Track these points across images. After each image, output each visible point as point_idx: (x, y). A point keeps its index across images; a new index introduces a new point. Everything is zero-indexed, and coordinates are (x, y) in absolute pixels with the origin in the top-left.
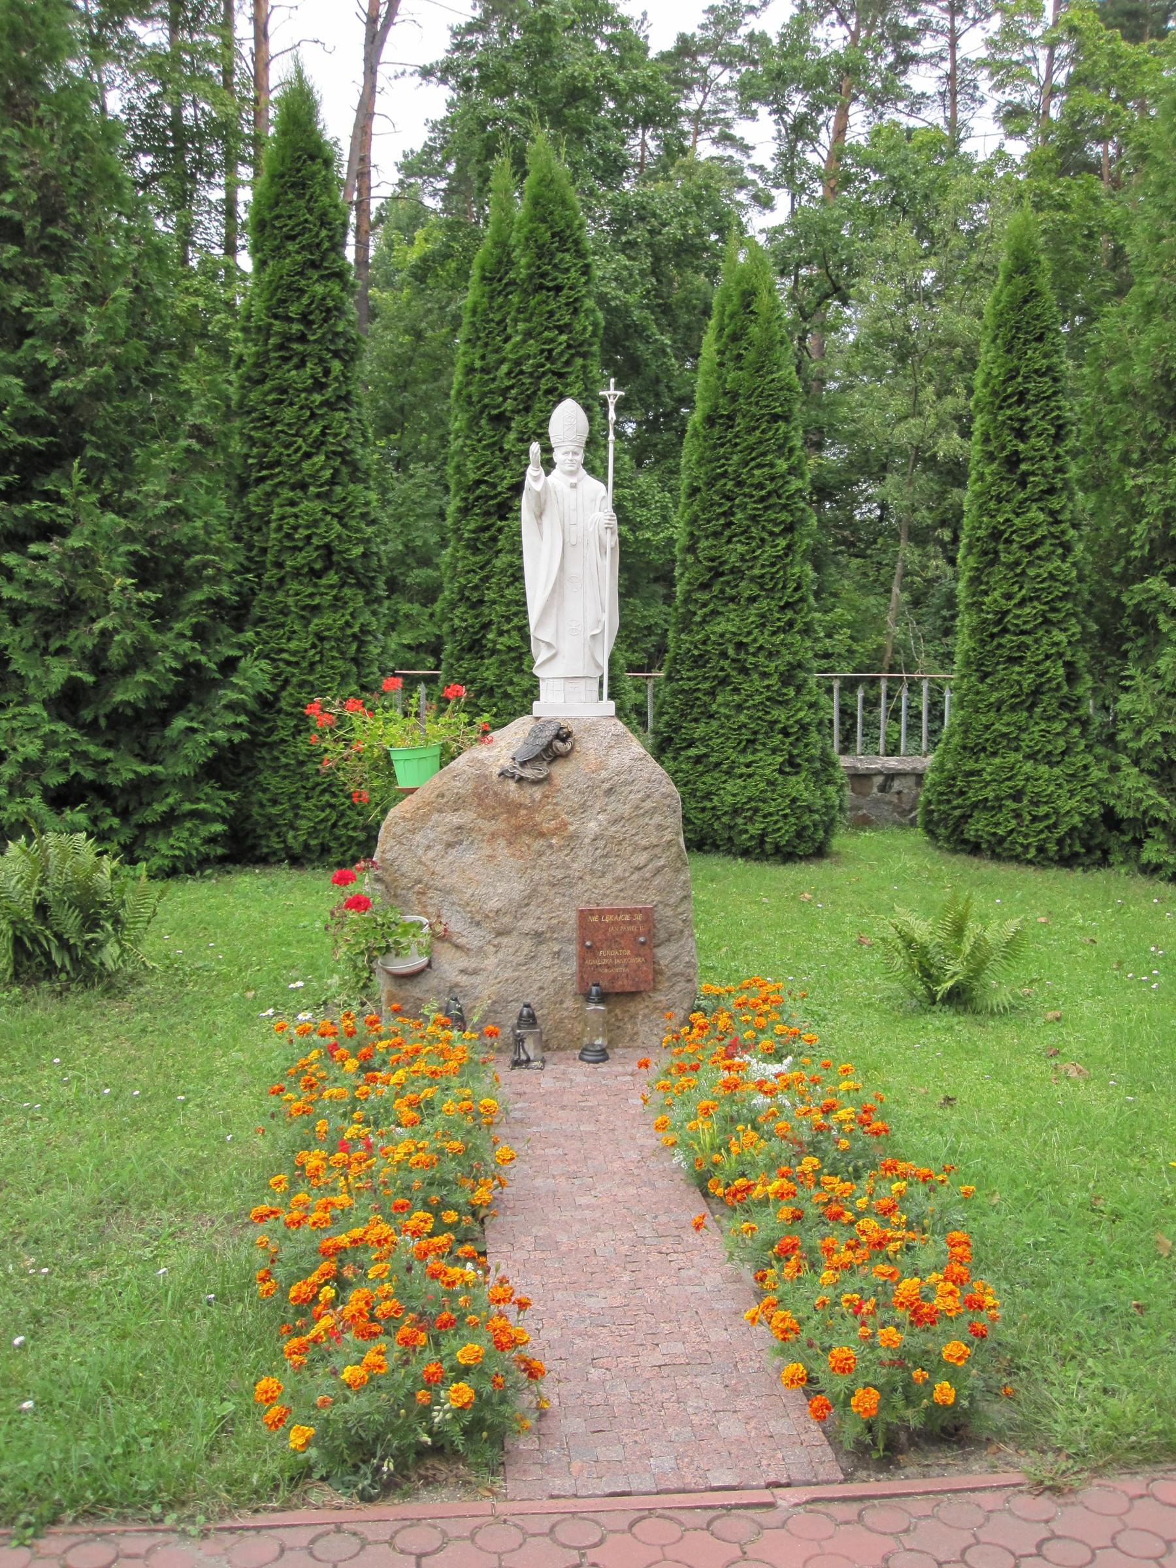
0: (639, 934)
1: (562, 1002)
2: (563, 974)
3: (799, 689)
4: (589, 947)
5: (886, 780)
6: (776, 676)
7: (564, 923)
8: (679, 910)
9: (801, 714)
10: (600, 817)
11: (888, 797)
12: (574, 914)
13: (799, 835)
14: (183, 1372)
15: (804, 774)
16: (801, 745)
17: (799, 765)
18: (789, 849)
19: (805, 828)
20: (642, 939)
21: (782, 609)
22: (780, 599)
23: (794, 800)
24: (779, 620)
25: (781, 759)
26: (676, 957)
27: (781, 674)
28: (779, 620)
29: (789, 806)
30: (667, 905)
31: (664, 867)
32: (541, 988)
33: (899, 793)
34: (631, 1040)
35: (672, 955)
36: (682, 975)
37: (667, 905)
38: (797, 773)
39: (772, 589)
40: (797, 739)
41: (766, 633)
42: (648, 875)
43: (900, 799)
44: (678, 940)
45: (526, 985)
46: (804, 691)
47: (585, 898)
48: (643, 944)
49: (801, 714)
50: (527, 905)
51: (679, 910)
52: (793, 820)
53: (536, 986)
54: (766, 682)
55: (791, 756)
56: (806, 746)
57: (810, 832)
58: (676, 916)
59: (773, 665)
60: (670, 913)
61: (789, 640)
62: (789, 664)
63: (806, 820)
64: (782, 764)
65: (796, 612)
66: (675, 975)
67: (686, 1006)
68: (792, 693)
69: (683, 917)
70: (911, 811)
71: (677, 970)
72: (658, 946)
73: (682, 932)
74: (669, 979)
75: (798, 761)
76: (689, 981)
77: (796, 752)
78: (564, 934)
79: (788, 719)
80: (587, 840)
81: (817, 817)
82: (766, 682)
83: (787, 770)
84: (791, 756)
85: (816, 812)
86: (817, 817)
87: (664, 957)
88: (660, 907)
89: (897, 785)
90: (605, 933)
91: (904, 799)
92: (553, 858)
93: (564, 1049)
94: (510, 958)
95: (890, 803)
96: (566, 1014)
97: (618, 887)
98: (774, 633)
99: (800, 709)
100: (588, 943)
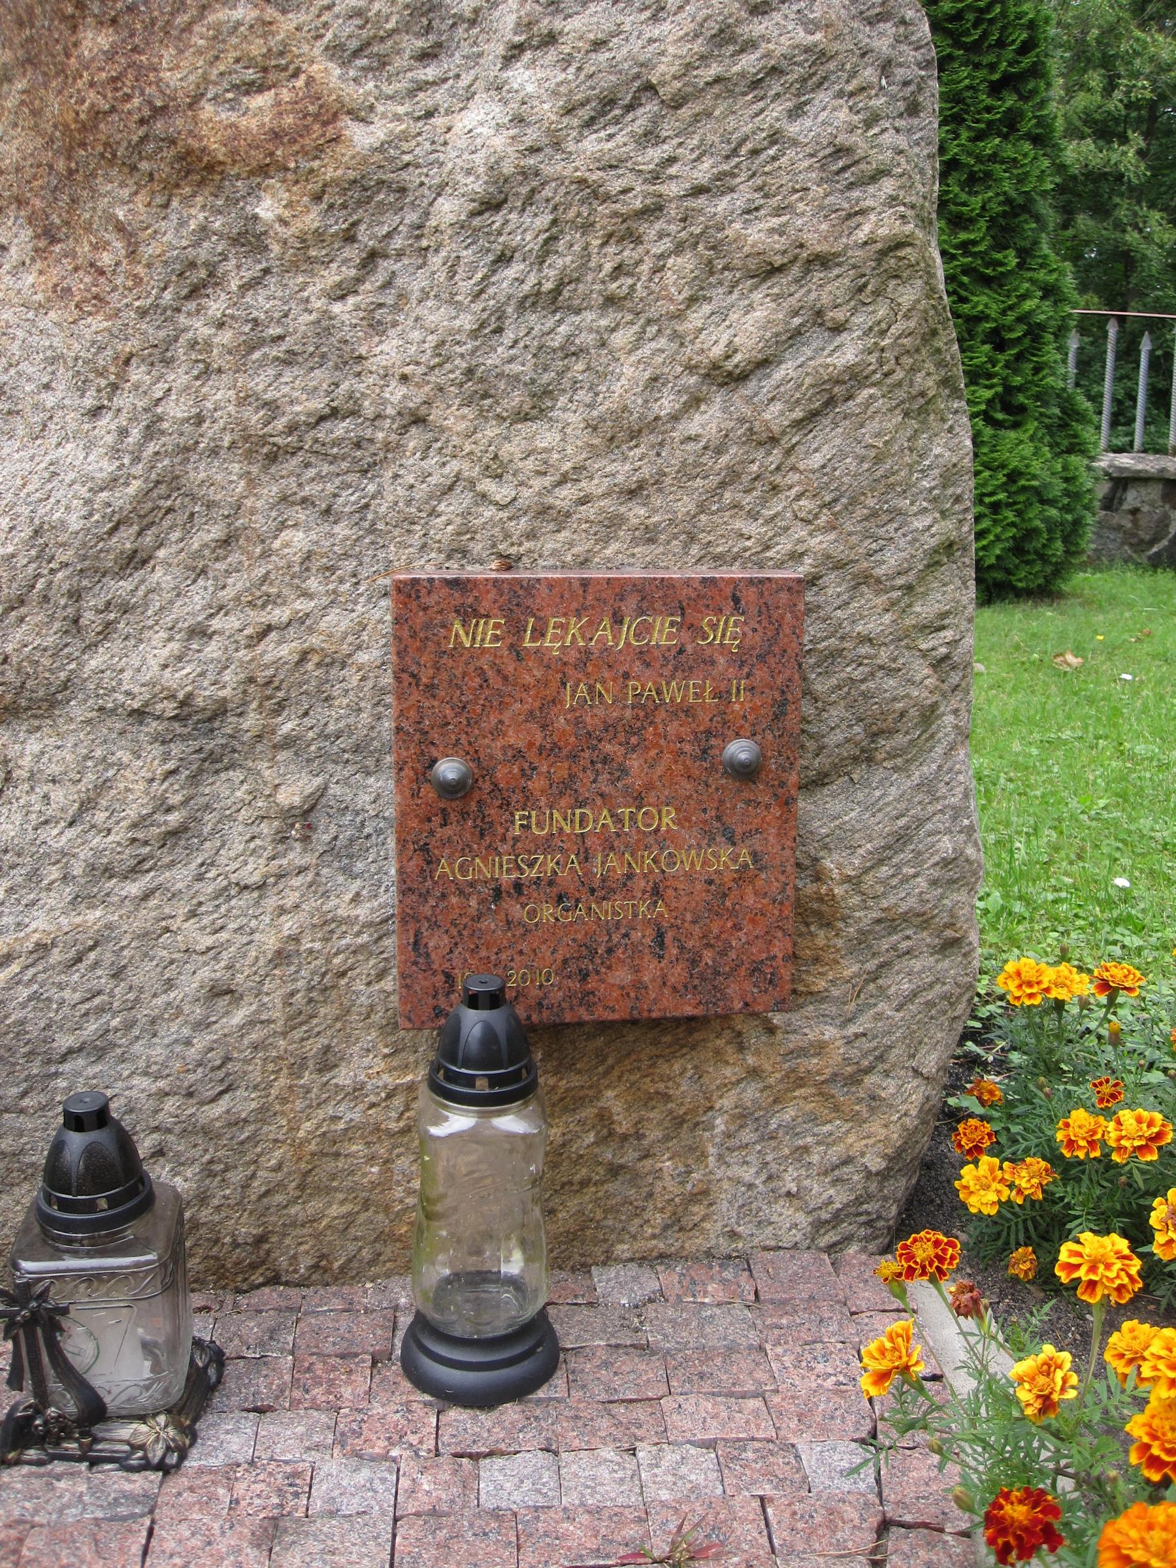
0: (728, 728)
1: (327, 1062)
2: (329, 925)
3: (1025, 254)
4: (450, 790)
5: (1114, 490)
6: (983, 224)
7: (333, 662)
8: (924, 610)
9: (1028, 305)
10: (523, 77)
11: (1116, 519)
12: (382, 613)
13: (1018, 549)
14: (681, 752)
15: (1032, 426)
16: (1028, 367)
17: (1022, 409)
18: (999, 576)
19: (1032, 533)
20: (740, 750)
21: (996, 89)
22: (992, 67)
23: (1013, 476)
24: (988, 109)
25: (988, 394)
26: (902, 838)
27: (992, 220)
28: (988, 109)
29: (1003, 487)
30: (864, 579)
31: (855, 377)
32: (219, 992)
33: (1135, 512)
34: (676, 1224)
35: (882, 826)
36: (923, 920)
37: (864, 579)
38: (1016, 426)
39: (975, 47)
40: (1019, 357)
41: (965, 134)
42: (775, 415)
43: (1135, 522)
44: (905, 759)
45: (144, 974)
46: (1034, 263)
47: (443, 529)
48: (746, 773)
49: (1028, 305)
50: (136, 560)
51: (924, 610)
52: (1010, 515)
53: (193, 982)
54: (963, 236)
55: (1009, 390)
56: (1037, 370)
57: (1037, 544)
58: (903, 637)
59: (976, 202)
60: (877, 623)
61: (1009, 151)
62: (1009, 201)
63: (1036, 517)
64: (990, 402)
65: (1024, 98)
66: (891, 922)
67: (931, 1061)
68: (1013, 261)
69: (935, 643)
70: (1152, 543)
71: (903, 900)
72: (818, 782)
73: (929, 715)
74: (862, 942)
75: (1021, 398)
76: (951, 945)
77: (1017, 380)
78: (332, 717)
79: (1004, 313)
80: (448, 209)
81: (1053, 512)
82: (963, 236)
83: (1000, 416)
84: (1009, 390)
85: (1051, 502)
86: (1053, 512)
87: (844, 840)
88: (834, 587)
89: (1132, 498)
90: (541, 717)
91: (1143, 522)
92: (261, 302)
93: (347, 1274)
94: (57, 838)
95: (1119, 528)
96: (352, 1114)
97: (622, 471)
98: (979, 136)
99: (1023, 297)
100: (449, 769)
